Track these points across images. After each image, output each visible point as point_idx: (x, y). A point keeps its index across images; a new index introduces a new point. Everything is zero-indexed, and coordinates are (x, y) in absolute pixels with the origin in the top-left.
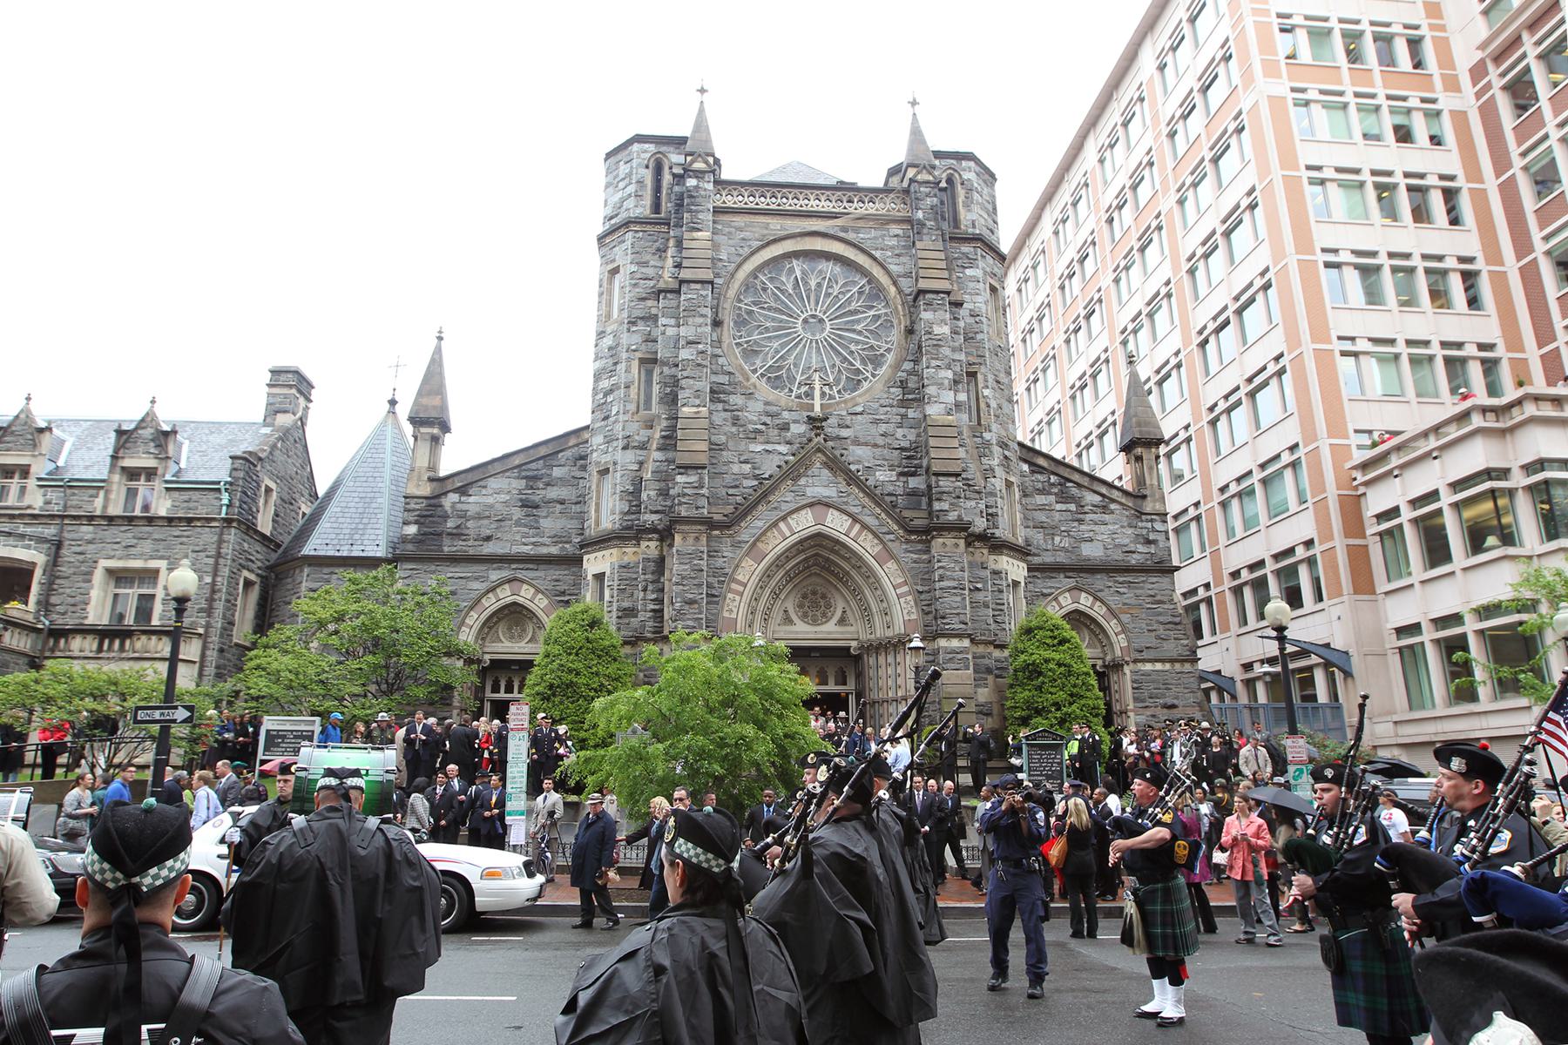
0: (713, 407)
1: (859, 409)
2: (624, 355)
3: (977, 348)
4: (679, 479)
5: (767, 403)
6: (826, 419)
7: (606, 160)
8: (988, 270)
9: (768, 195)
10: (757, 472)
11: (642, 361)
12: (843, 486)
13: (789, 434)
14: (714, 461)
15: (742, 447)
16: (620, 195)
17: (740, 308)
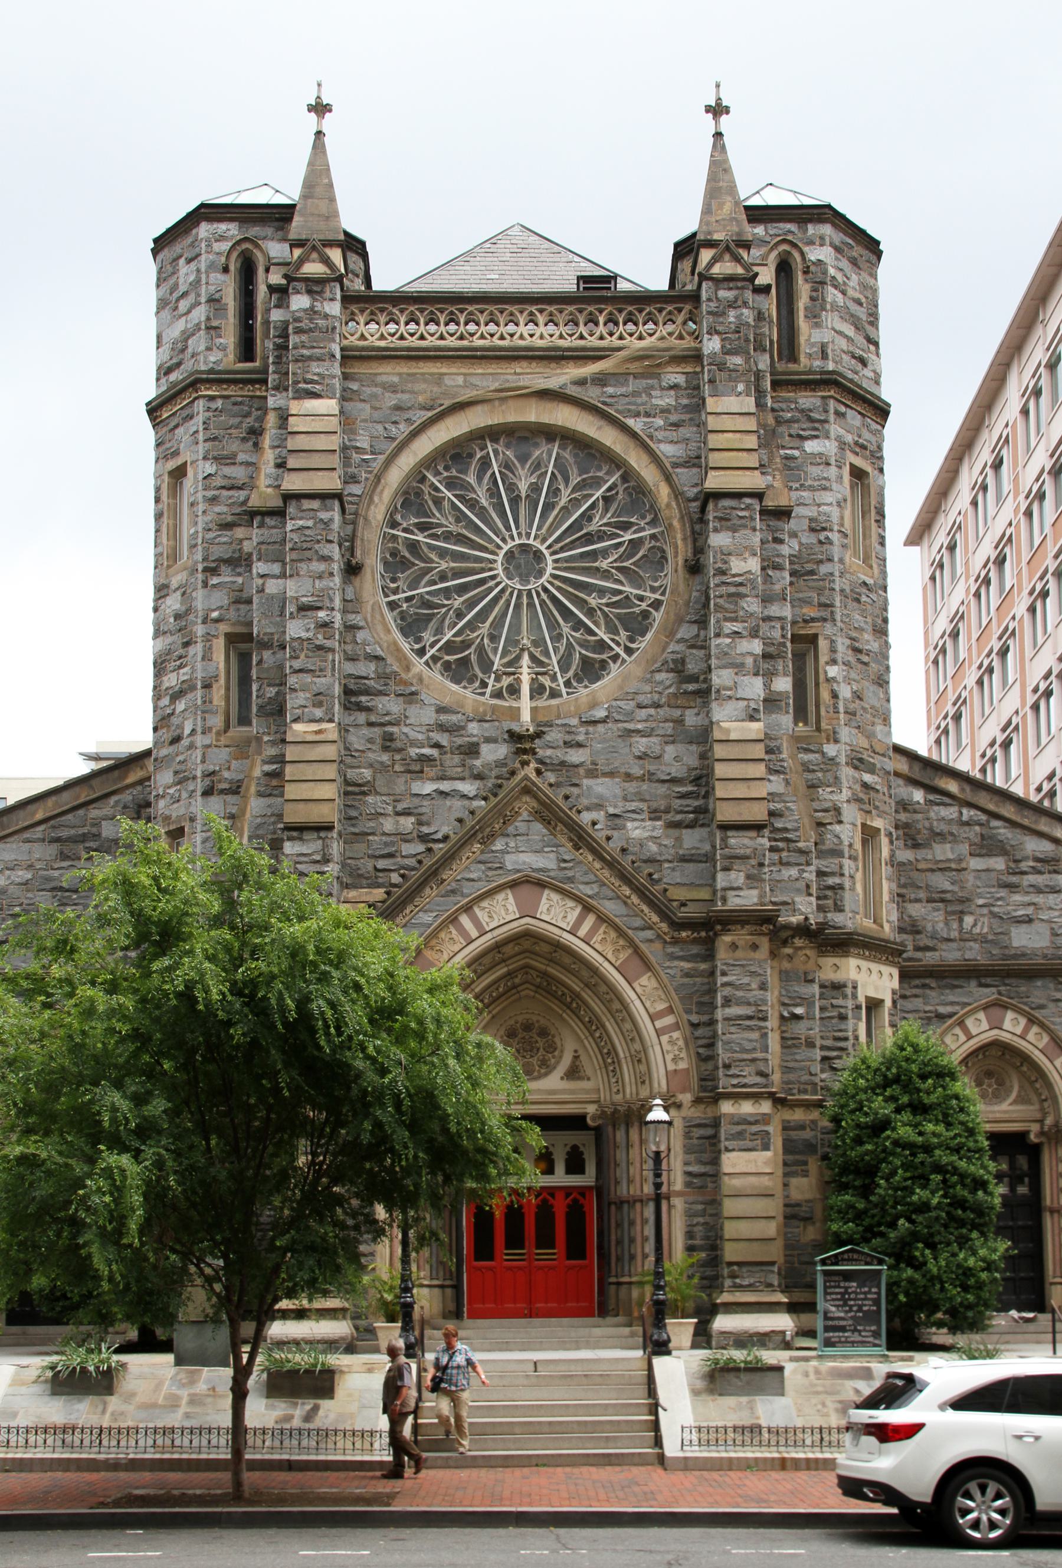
0: (348, 720)
1: (601, 713)
2: (200, 630)
3: (820, 591)
4: (289, 848)
5: (441, 710)
6: (539, 735)
7: (155, 252)
8: (849, 438)
9: (442, 319)
10: (425, 830)
11: (232, 639)
12: (567, 851)
13: (478, 763)
14: (354, 813)
15: (400, 786)
16: (181, 325)
17: (394, 538)
